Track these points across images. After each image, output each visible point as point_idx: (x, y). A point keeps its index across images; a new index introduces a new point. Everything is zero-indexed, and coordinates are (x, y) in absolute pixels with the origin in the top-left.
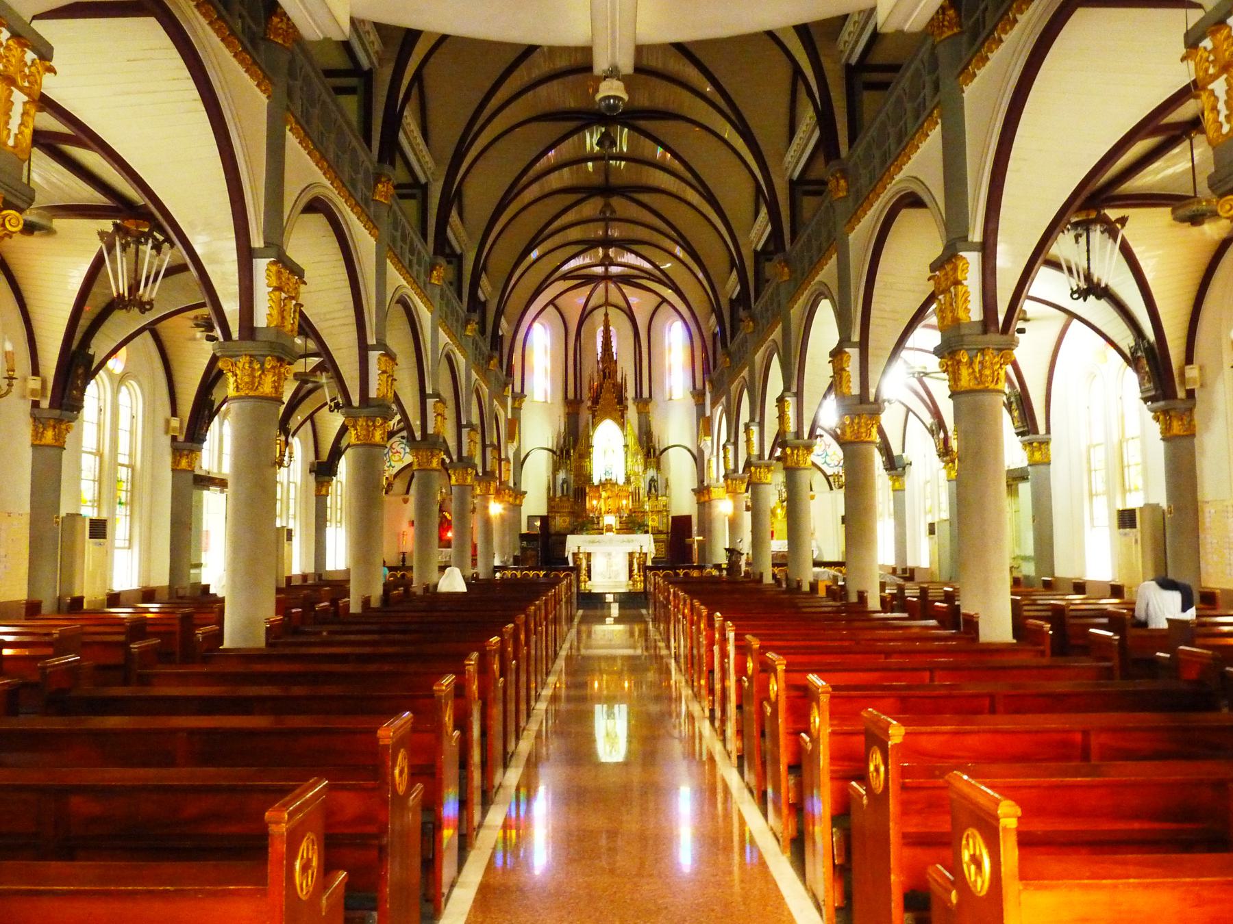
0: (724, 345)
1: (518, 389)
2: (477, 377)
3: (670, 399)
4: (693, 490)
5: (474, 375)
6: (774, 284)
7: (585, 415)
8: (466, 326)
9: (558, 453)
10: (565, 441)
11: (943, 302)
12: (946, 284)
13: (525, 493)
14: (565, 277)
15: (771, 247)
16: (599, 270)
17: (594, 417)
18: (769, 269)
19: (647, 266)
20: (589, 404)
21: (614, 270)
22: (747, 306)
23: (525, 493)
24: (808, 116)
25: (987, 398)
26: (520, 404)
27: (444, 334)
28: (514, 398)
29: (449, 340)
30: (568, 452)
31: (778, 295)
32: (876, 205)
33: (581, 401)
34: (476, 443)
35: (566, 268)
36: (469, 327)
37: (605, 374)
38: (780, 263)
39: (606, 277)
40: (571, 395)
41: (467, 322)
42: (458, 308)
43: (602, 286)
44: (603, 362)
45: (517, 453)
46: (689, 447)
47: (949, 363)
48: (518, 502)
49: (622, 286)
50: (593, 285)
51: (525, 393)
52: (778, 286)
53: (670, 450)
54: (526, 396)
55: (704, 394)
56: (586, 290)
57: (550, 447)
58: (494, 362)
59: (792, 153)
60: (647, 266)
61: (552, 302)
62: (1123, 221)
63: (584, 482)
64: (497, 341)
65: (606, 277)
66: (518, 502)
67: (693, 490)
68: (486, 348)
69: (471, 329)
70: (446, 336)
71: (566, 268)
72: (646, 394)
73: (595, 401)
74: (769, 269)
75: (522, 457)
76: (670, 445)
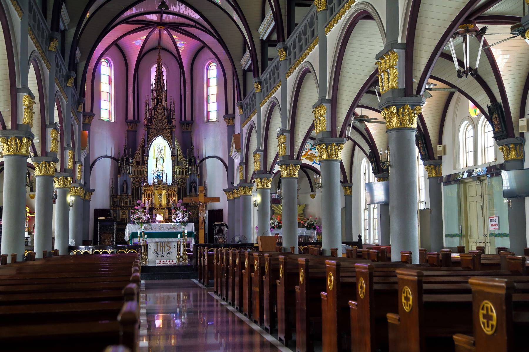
0: (239, 99)
1: (88, 109)
2: (58, 89)
3: (208, 121)
4: (225, 190)
5: (57, 88)
6: (276, 61)
7: (142, 132)
8: (50, 43)
9: (120, 161)
10: (125, 152)
11: (383, 77)
12: (385, 68)
13: (93, 191)
14: (126, 21)
15: (275, 37)
16: (154, 17)
17: (149, 133)
18: (271, 52)
19: (196, 16)
20: (145, 123)
21: (169, 18)
22: (256, 75)
23: (93, 191)
24: (269, 15)
25: (408, 132)
26: (90, 121)
27: (32, 42)
28: (84, 116)
29: (36, 49)
30: (128, 160)
31: (278, 69)
32: (344, 16)
33: (138, 122)
34: (58, 142)
35: (128, 13)
36: (52, 44)
37: (158, 100)
38: (280, 49)
39: (160, 24)
40: (130, 117)
41: (51, 39)
42: (43, 25)
43: (156, 32)
44: (156, 91)
45: (87, 159)
46: (221, 157)
47: (386, 113)
48: (87, 198)
49: (172, 32)
50: (151, 30)
51: (94, 112)
52: (278, 63)
53: (207, 160)
54: (94, 115)
55: (233, 118)
56: (147, 32)
57: (113, 155)
58: (71, 81)
59: (262, 28)
60: (196, 16)
61: (115, 43)
62: (484, 30)
63: (140, 184)
64: (73, 66)
65: (160, 24)
66: (87, 198)
67: (225, 190)
68: (65, 65)
69: (55, 45)
70: (34, 45)
71: (128, 13)
72: (188, 118)
73: (150, 121)
74: (271, 52)
75: (91, 163)
76: (207, 156)
